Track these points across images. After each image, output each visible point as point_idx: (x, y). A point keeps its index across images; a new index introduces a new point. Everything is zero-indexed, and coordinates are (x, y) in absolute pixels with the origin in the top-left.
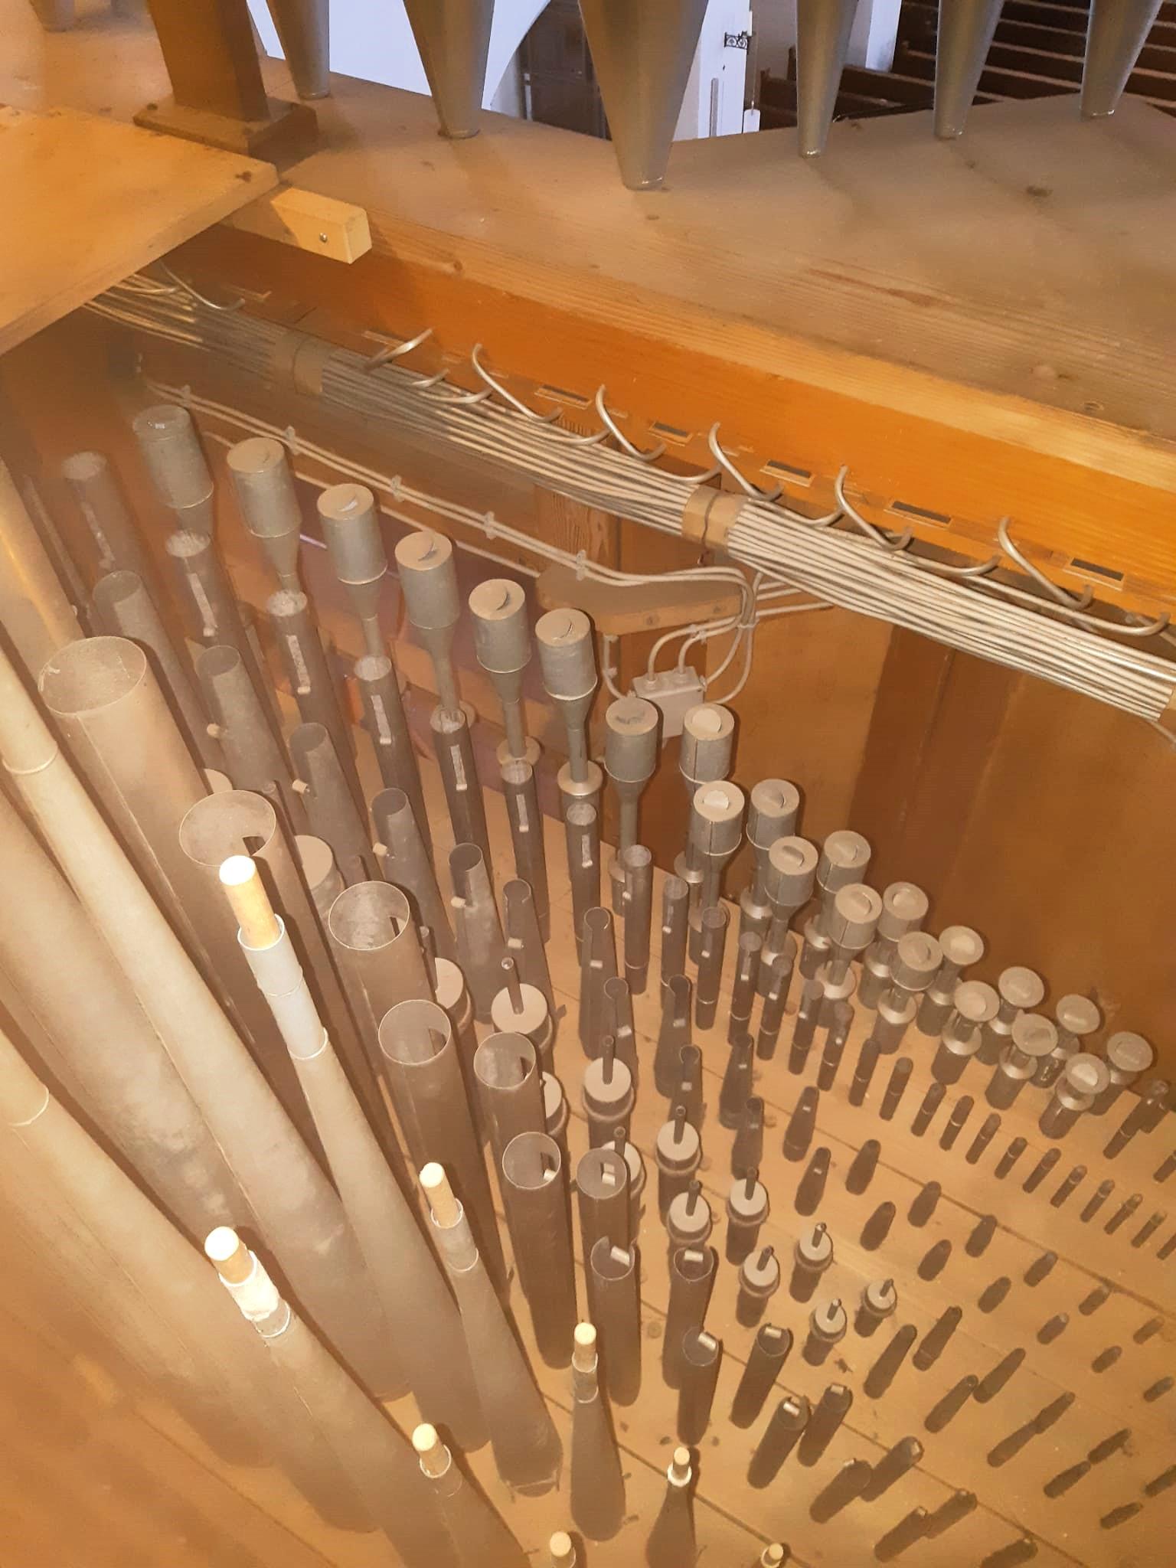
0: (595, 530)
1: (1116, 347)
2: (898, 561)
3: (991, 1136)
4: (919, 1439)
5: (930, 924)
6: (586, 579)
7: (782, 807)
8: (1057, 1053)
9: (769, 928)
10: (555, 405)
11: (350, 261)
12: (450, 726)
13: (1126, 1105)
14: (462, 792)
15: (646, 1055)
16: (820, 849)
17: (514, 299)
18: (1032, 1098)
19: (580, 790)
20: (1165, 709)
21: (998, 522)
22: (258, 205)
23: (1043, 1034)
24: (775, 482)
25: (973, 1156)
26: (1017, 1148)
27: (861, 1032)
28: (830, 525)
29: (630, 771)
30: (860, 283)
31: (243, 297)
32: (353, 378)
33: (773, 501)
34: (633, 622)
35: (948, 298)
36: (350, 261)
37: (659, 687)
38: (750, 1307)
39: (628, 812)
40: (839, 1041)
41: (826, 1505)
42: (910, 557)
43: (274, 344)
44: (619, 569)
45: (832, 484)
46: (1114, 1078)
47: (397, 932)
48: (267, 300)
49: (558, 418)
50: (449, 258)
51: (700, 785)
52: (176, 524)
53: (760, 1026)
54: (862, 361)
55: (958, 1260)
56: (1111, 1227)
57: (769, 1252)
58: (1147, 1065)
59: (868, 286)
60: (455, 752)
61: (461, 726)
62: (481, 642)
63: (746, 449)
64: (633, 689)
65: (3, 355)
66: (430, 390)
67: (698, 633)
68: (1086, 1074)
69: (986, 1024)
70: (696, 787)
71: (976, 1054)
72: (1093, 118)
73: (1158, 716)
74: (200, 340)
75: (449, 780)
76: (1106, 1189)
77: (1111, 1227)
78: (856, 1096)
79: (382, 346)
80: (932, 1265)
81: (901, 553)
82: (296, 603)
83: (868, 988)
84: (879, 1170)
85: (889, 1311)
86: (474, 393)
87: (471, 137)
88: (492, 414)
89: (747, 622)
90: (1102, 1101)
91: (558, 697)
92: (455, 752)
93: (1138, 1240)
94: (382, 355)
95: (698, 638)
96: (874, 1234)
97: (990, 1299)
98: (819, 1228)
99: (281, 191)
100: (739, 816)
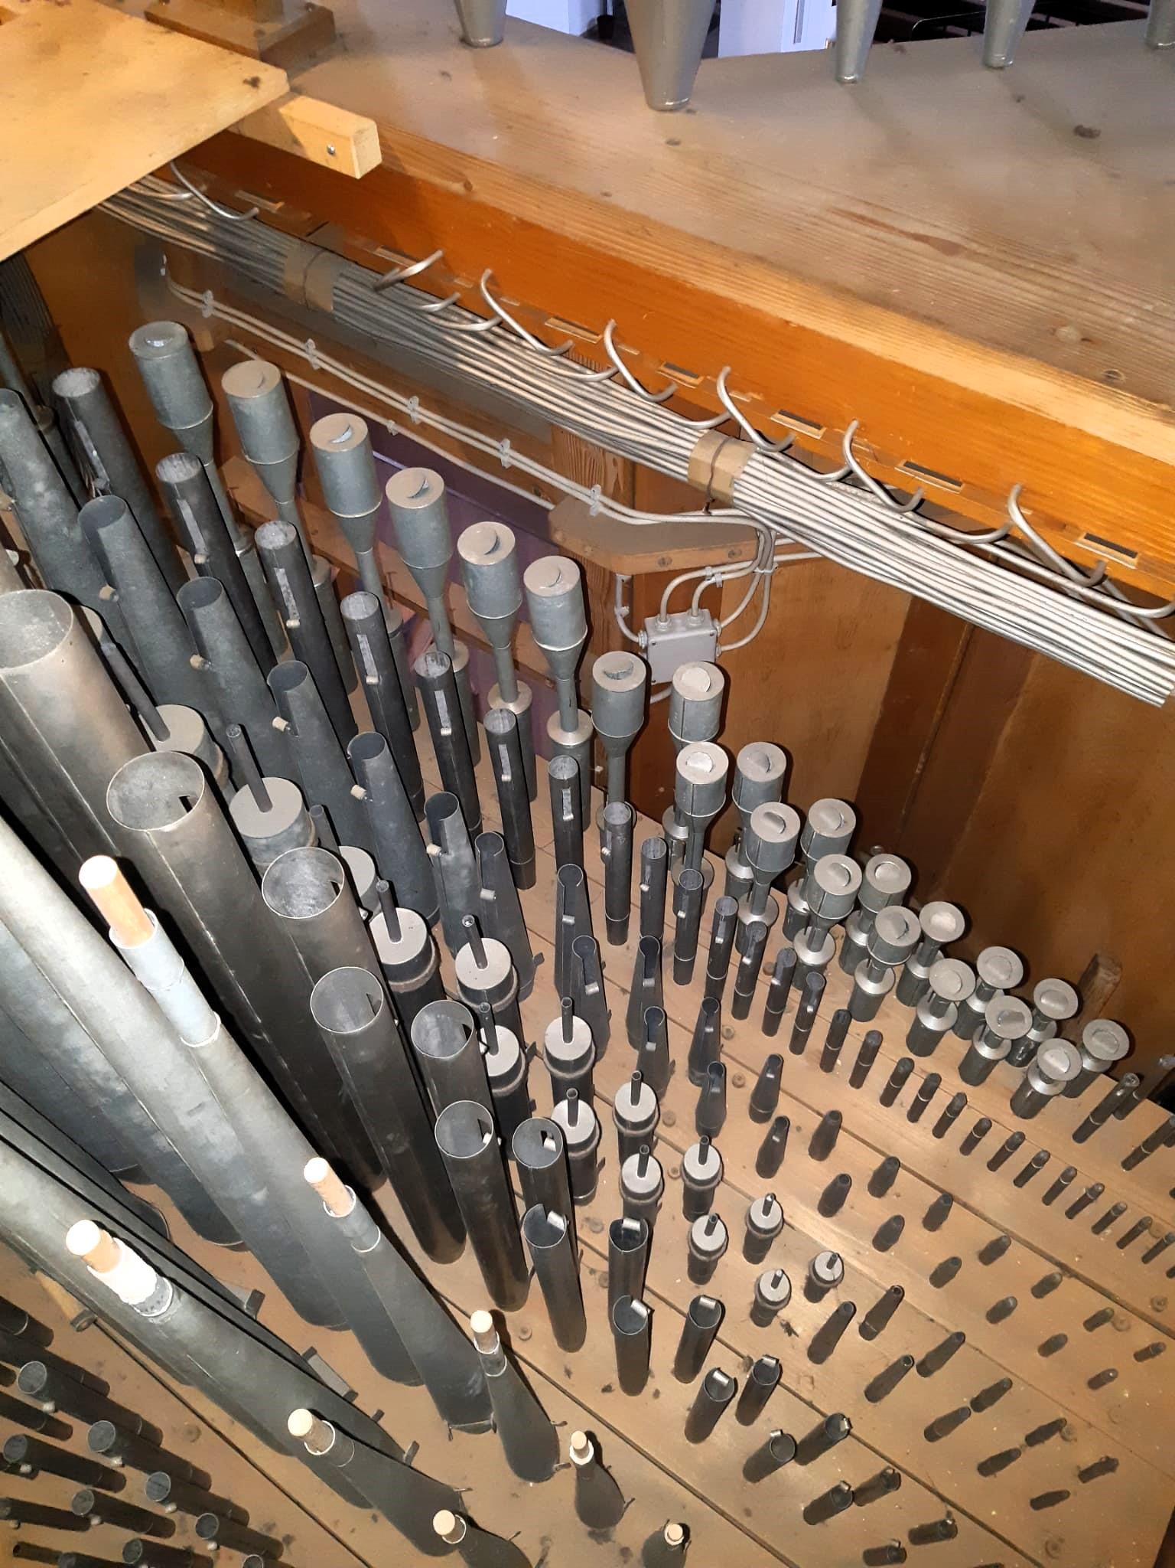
0: (610, 466)
1: (1147, 310)
2: (906, 522)
3: (957, 1113)
4: (847, 1416)
5: (913, 898)
6: (601, 514)
7: (768, 770)
8: (1033, 1035)
9: (751, 889)
10: (566, 337)
11: (358, 176)
12: (436, 671)
13: (1104, 1086)
14: (446, 737)
15: (618, 1006)
16: (803, 818)
17: (525, 225)
18: (1006, 1076)
19: (571, 740)
20: (1169, 696)
21: (1008, 491)
22: (264, 114)
23: (1019, 1017)
24: (786, 431)
25: (940, 1130)
26: (982, 1128)
27: (835, 1001)
28: (840, 480)
29: (620, 727)
30: (884, 225)
31: (257, 206)
32: (364, 297)
33: (782, 452)
34: (647, 563)
35: (974, 246)
36: (358, 176)
37: (671, 629)
38: (701, 1268)
39: (616, 767)
40: (810, 1009)
41: (760, 1466)
42: (920, 520)
43: (286, 257)
44: (633, 507)
45: (842, 437)
46: (1088, 1064)
47: (337, 890)
48: (280, 209)
49: (568, 351)
50: (458, 177)
51: (688, 744)
52: (173, 445)
53: (735, 987)
54: (873, 312)
55: (914, 1233)
56: (1072, 1212)
57: (716, 1218)
58: (1123, 1054)
59: (890, 229)
60: (440, 696)
61: (447, 669)
62: (469, 585)
63: (756, 396)
64: (645, 630)
65: (4, 262)
66: (441, 314)
67: (713, 575)
68: (1058, 1060)
69: (964, 1003)
70: (683, 745)
71: (953, 1028)
72: (1157, 47)
73: (1162, 701)
74: (212, 249)
75: (435, 725)
76: (1069, 1175)
77: (1072, 1212)
78: (828, 1062)
79: (391, 266)
80: (886, 1237)
81: (910, 514)
82: (286, 535)
83: (850, 955)
84: (842, 1138)
85: (834, 1283)
86: (486, 320)
87: (494, 45)
88: (501, 343)
89: (765, 567)
90: (1075, 1087)
91: (545, 646)
92: (440, 696)
93: (1099, 1228)
94: (390, 277)
95: (713, 580)
96: (832, 1201)
97: (943, 1275)
98: (769, 1199)
99: (292, 99)
100: (721, 780)
